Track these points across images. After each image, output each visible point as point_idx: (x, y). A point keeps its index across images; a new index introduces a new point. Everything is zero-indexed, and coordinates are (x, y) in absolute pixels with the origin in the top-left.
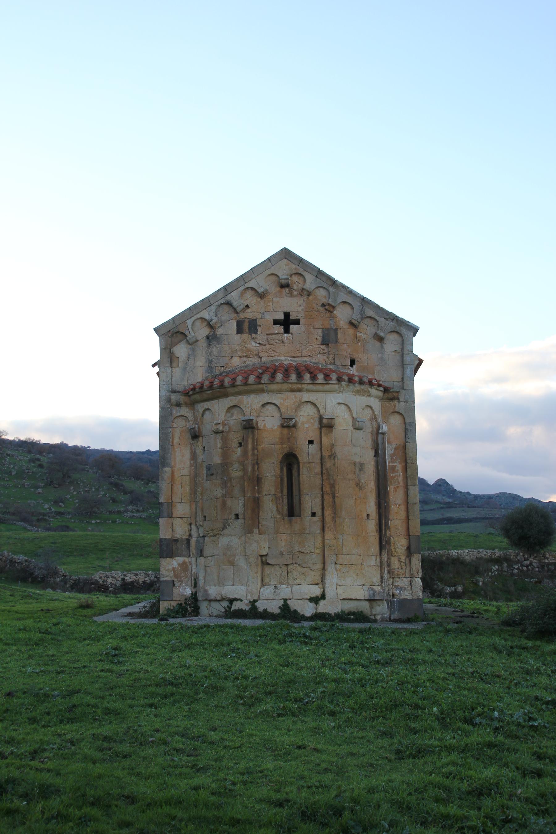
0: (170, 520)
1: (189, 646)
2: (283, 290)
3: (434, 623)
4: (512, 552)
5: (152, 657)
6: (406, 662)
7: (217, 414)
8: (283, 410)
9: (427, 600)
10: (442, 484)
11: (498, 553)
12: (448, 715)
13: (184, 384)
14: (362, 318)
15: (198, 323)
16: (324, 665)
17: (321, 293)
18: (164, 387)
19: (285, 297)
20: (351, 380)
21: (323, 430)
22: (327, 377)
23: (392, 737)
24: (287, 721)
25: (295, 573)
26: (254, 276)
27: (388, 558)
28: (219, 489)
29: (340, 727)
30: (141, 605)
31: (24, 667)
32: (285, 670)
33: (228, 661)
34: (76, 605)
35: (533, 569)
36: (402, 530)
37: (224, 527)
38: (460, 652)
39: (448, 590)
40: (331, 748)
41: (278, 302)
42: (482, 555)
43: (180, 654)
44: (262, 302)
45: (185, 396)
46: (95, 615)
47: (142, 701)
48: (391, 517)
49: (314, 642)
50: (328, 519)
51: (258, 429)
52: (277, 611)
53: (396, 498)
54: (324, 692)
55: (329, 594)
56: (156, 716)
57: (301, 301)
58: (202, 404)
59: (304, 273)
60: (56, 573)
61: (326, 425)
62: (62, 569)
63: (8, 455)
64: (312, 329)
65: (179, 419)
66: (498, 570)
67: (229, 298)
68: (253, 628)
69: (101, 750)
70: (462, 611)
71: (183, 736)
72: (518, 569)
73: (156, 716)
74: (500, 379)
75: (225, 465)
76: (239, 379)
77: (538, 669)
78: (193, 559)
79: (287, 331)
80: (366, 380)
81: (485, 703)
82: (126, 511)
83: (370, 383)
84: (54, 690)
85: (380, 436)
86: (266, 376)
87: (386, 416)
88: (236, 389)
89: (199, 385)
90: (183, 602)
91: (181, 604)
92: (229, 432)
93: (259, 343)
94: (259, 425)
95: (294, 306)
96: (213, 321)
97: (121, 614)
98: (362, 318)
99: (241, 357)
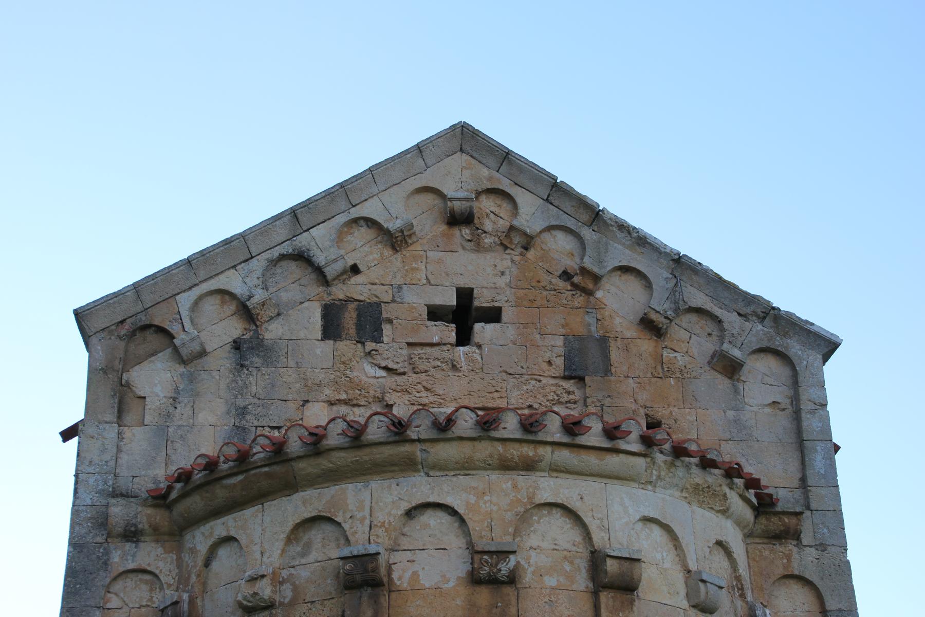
2: (456, 231)
7: (257, 548)
8: (473, 525)
15: (211, 306)
17: (561, 244)
18: (92, 481)
19: (461, 251)
26: (375, 190)
41: (439, 262)
44: (397, 260)
45: (154, 506)
57: (504, 261)
58: (205, 528)
64: (538, 336)
65: (130, 582)
67: (303, 241)
79: (464, 338)
88: (324, 463)
92: (293, 603)
93: (386, 368)
94: (395, 576)
95: (486, 273)
96: (255, 300)
98: (677, 310)
99: (331, 404)
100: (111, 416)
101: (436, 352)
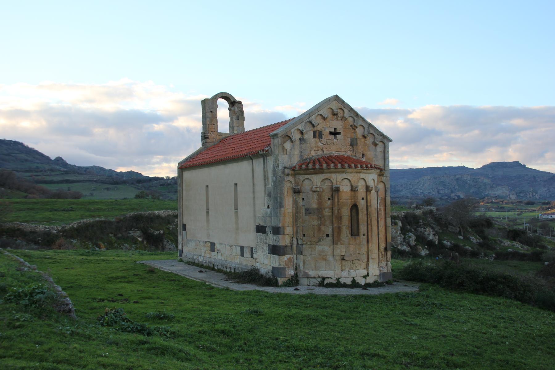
8: (352, 182)
15: (296, 132)
37: (320, 241)
42: (170, 213)
52: (350, 283)
59: (344, 109)
67: (310, 119)
74: (91, 101)
75: (320, 210)
88: (329, 171)
95: (338, 125)
101: (330, 141)
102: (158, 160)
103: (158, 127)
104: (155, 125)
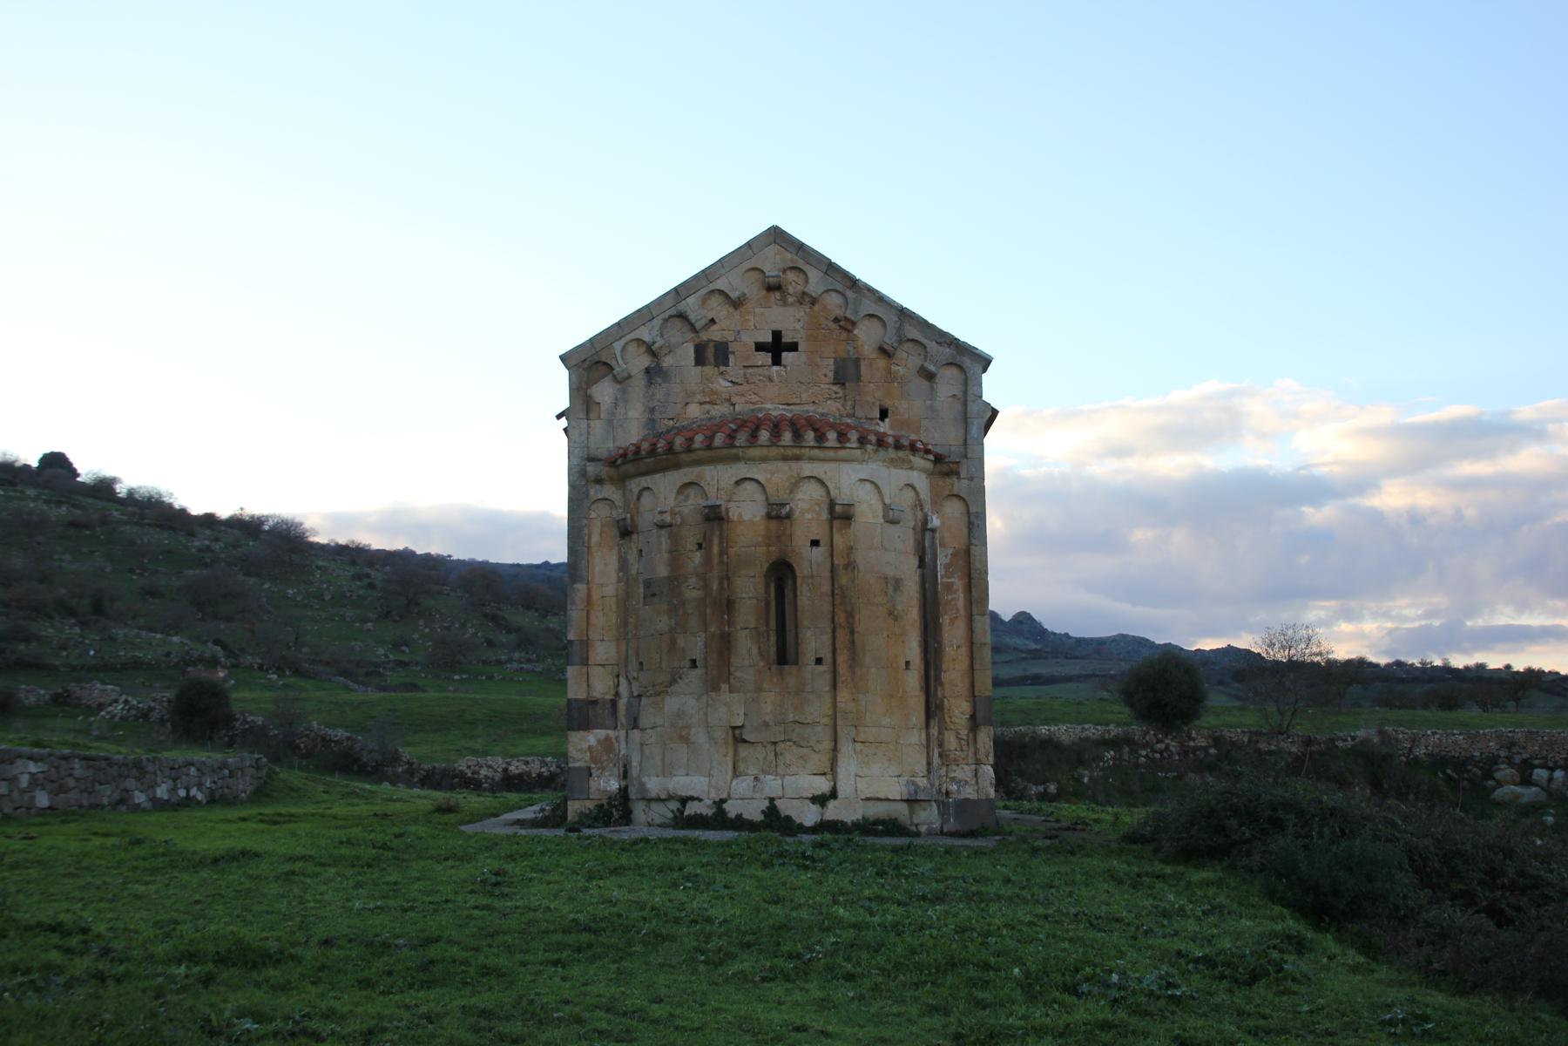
0: (584, 670)
1: (617, 871)
3: (1012, 838)
4: (1136, 730)
5: (556, 887)
6: (968, 897)
9: (1001, 804)
10: (1024, 621)
11: (1114, 730)
12: (1037, 980)
13: (606, 446)
14: (900, 342)
15: (632, 348)
16: (835, 902)
17: (834, 300)
20: (881, 443)
21: (836, 523)
22: (842, 437)
23: (947, 1014)
24: (777, 989)
25: (788, 756)
27: (940, 733)
28: (665, 619)
29: (861, 998)
30: (536, 808)
31: (348, 900)
32: (772, 909)
33: (679, 895)
34: (430, 807)
35: (1170, 756)
36: (962, 687)
37: (673, 681)
38: (1056, 883)
39: (1034, 790)
40: (849, 1031)
43: (601, 883)
44: (737, 314)
46: (462, 823)
47: (541, 956)
48: (944, 666)
49: (820, 865)
50: (842, 668)
51: (728, 520)
53: (953, 635)
54: (836, 943)
55: (844, 789)
56: (564, 979)
57: (801, 312)
59: (806, 268)
60: (396, 758)
61: (840, 515)
62: (406, 752)
63: (319, 568)
65: (601, 505)
66: (1113, 758)
67: (682, 306)
68: (720, 844)
69: (476, 1030)
70: (1058, 821)
71: (607, 1011)
72: (1146, 756)
73: (564, 979)
74: (1121, 451)
75: (675, 580)
76: (699, 438)
77: (1182, 908)
78: (623, 733)
80: (906, 443)
81: (1098, 960)
82: (510, 660)
83: (913, 448)
84: (398, 937)
85: (928, 535)
86: (742, 435)
87: (938, 500)
88: (693, 456)
89: (632, 448)
90: (605, 802)
91: (602, 806)
95: (789, 321)
97: (508, 821)
98: (900, 342)
100: (582, 415)
101: (760, 370)
102: (1322, 614)
103: (1317, 515)
104: (1307, 510)
